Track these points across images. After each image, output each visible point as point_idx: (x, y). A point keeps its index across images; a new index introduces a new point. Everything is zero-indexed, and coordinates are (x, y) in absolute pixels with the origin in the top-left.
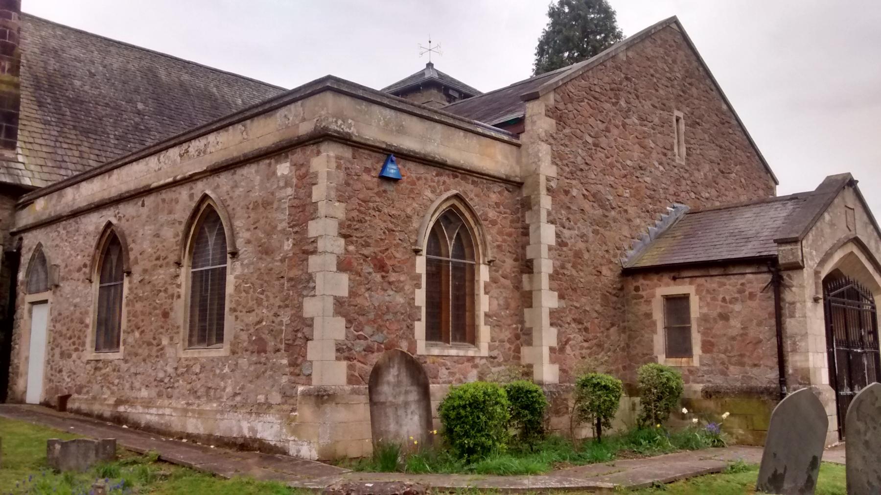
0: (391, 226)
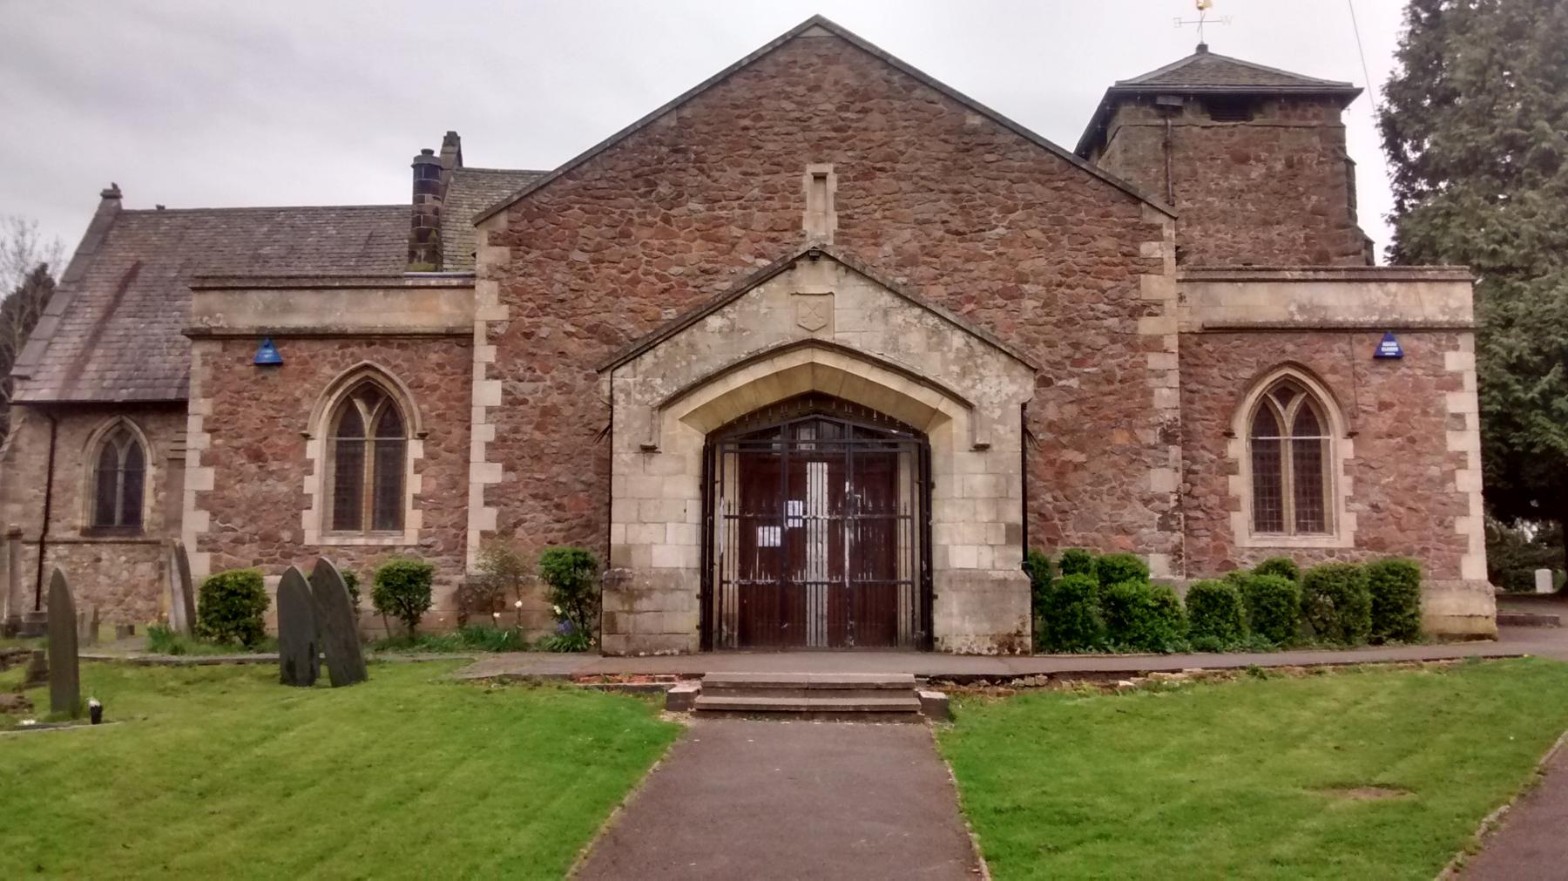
0: (272, 413)
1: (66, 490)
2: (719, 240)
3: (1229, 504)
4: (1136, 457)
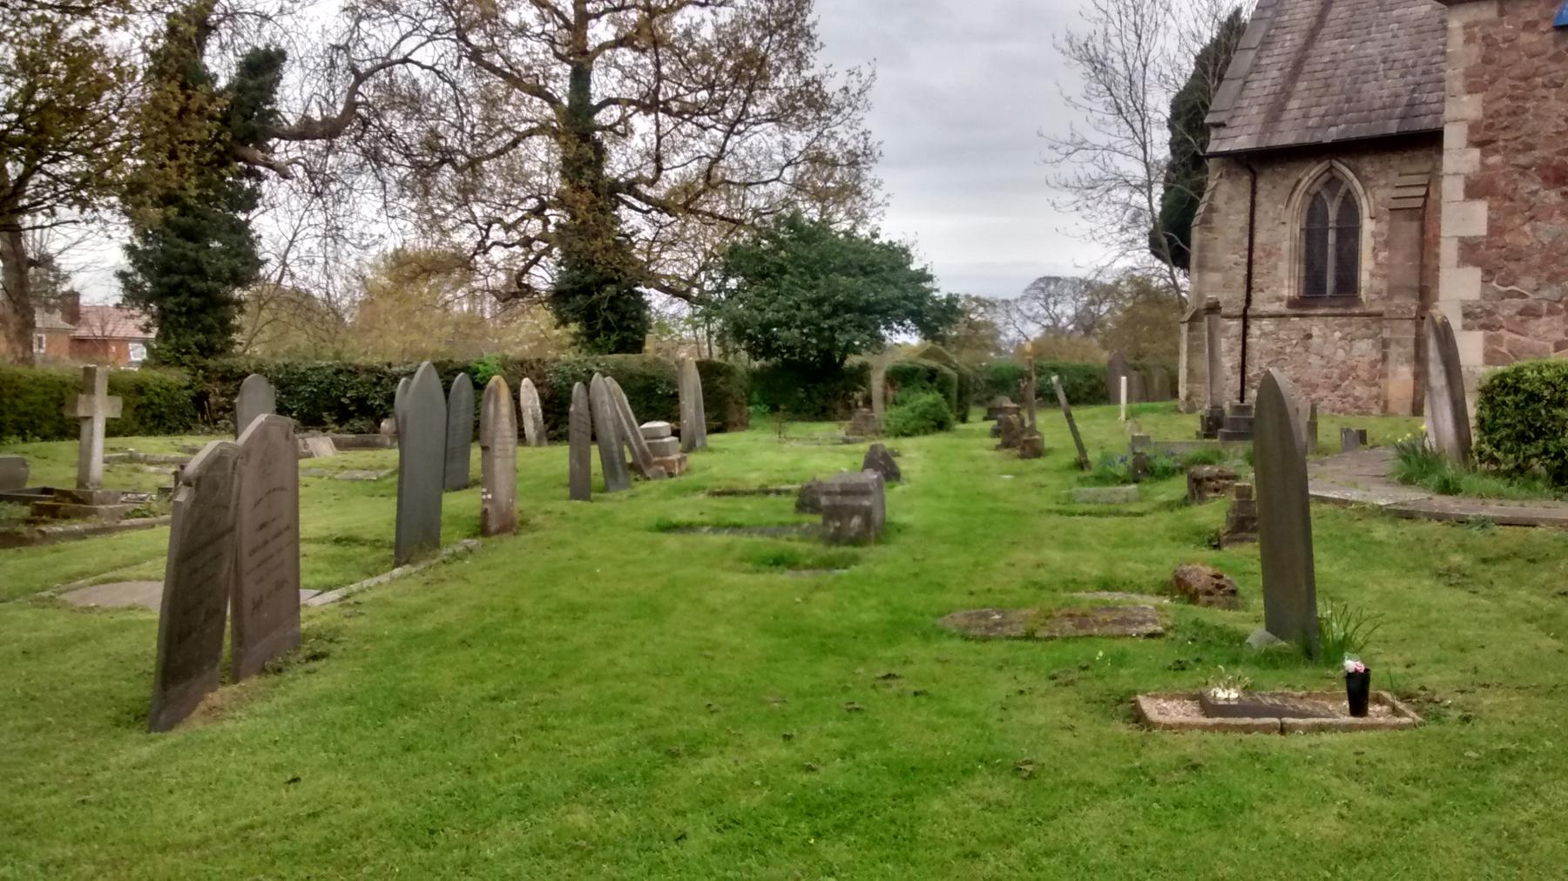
1: (1269, 255)
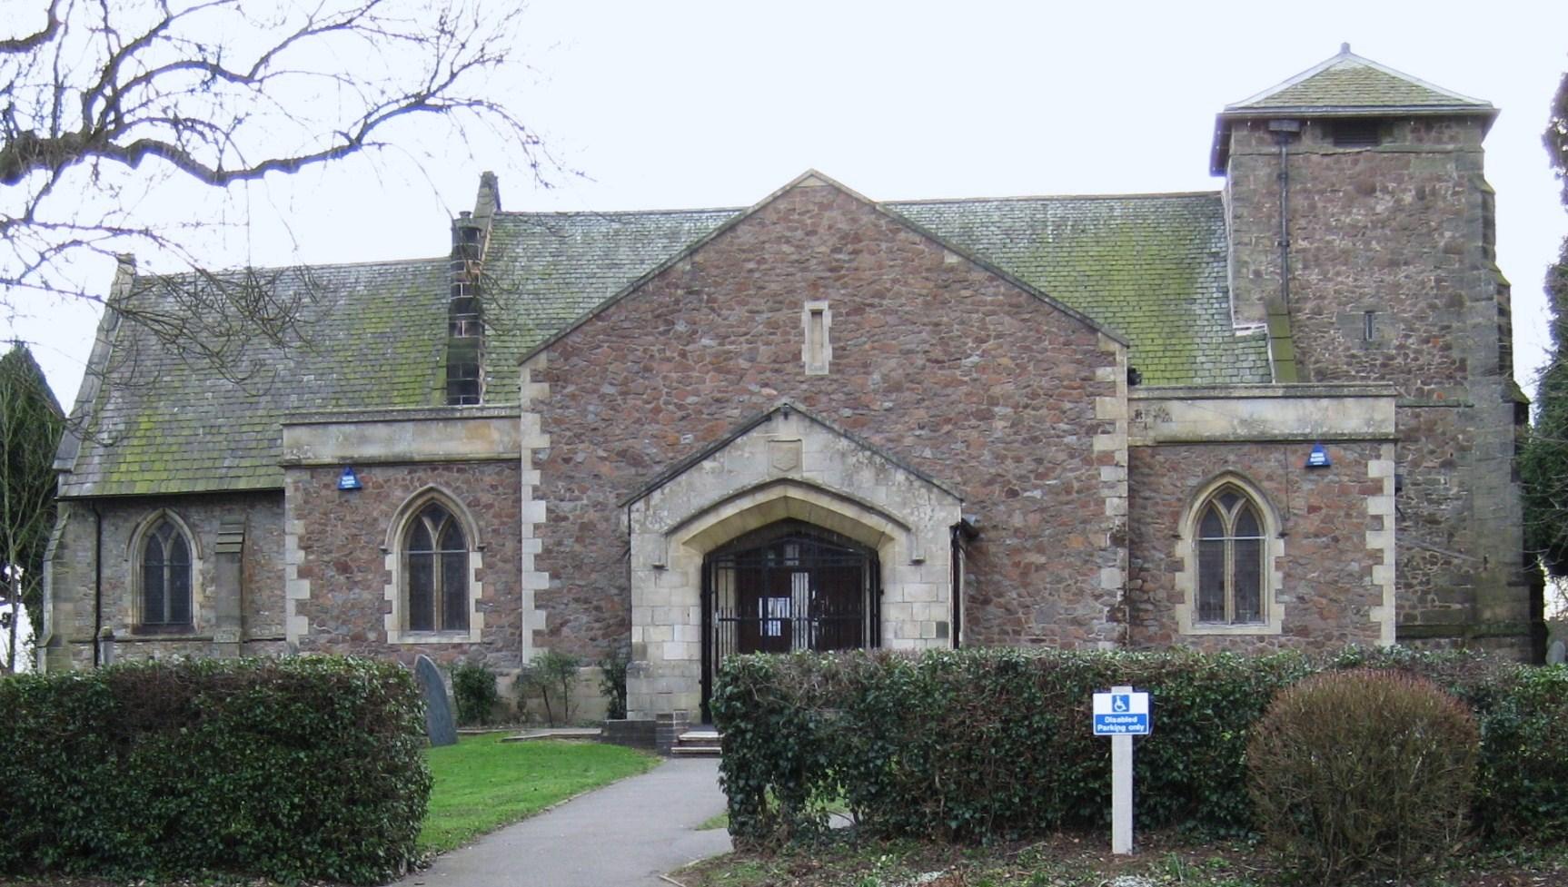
1: (114, 587)
2: (729, 372)
3: (1177, 597)
4: (1089, 561)
